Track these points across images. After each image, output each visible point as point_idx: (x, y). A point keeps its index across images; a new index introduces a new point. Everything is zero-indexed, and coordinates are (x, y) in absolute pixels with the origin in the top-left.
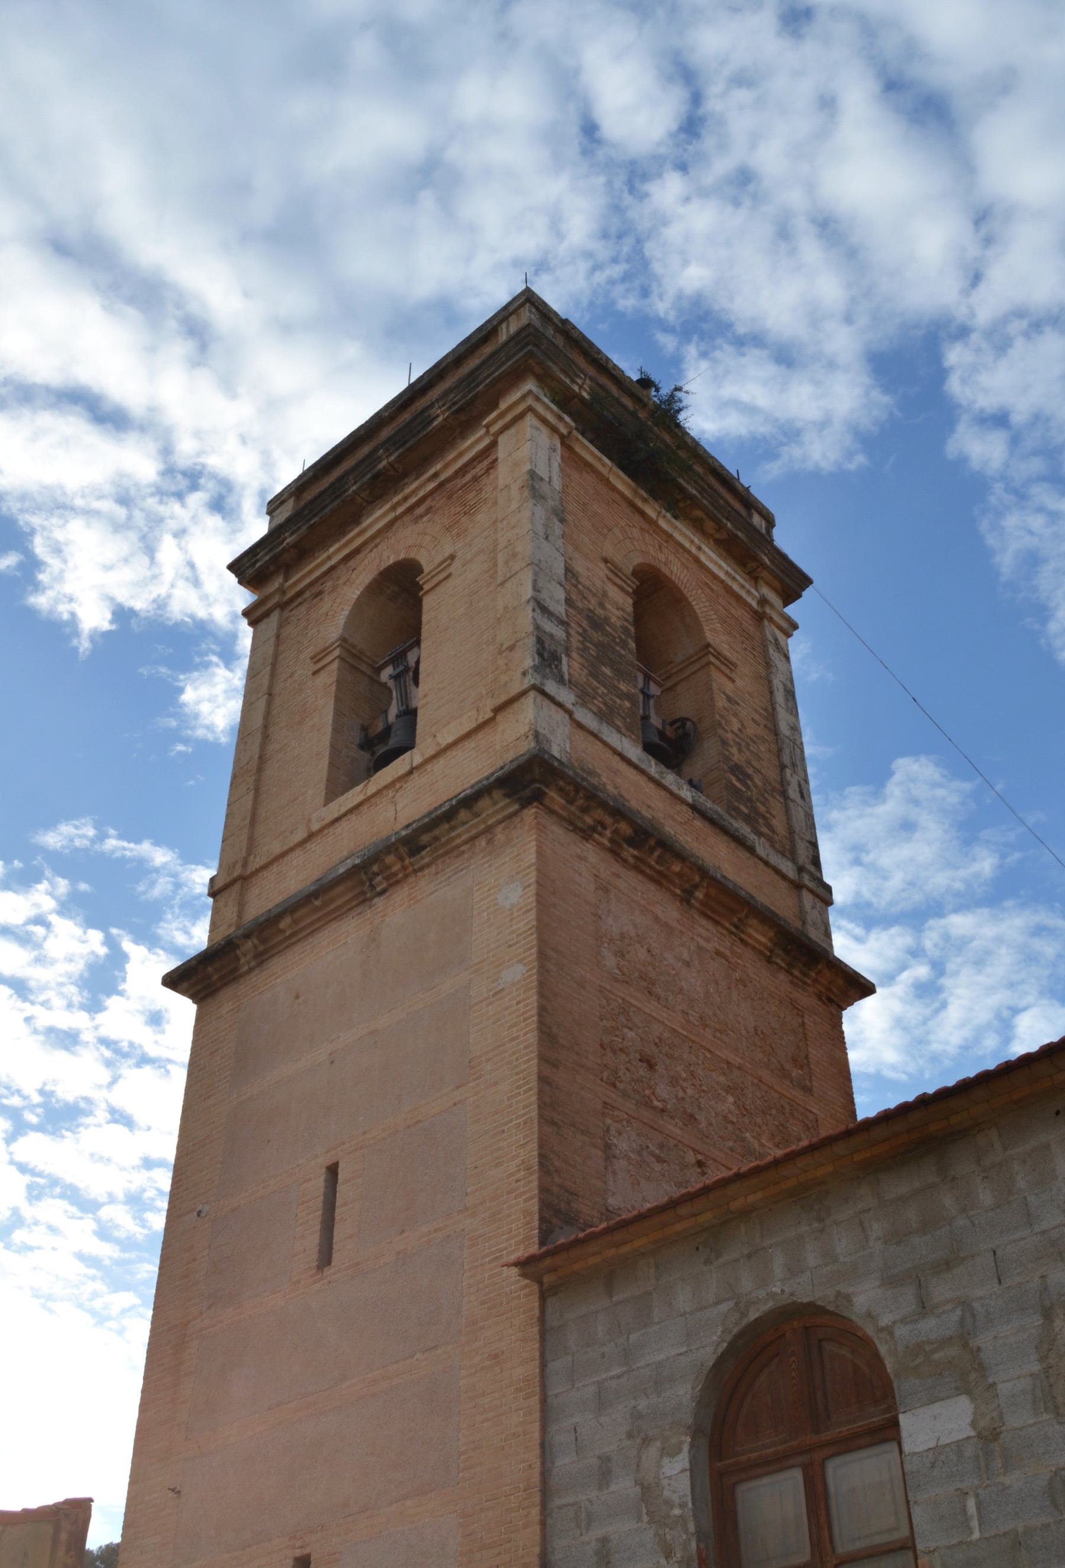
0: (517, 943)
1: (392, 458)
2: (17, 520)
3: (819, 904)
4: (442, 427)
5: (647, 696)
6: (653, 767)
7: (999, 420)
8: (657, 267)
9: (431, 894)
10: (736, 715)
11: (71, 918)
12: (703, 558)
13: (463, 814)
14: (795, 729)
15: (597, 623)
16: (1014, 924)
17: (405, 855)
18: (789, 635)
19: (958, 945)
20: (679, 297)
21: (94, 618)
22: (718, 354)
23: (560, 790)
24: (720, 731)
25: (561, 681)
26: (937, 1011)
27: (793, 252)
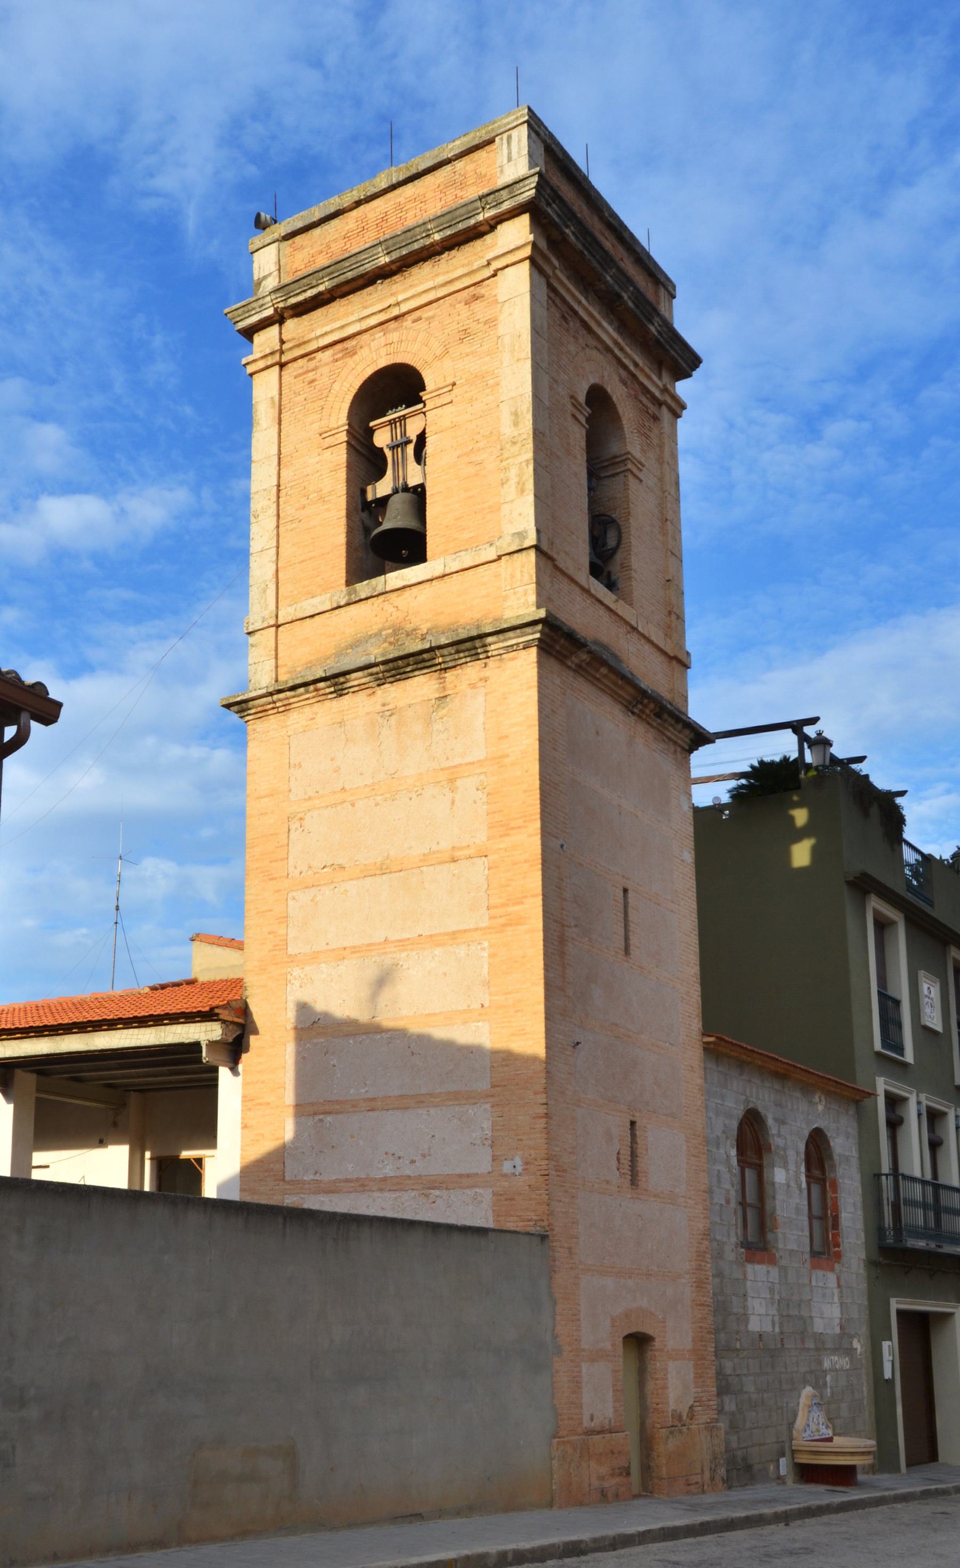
13: (680, 726)
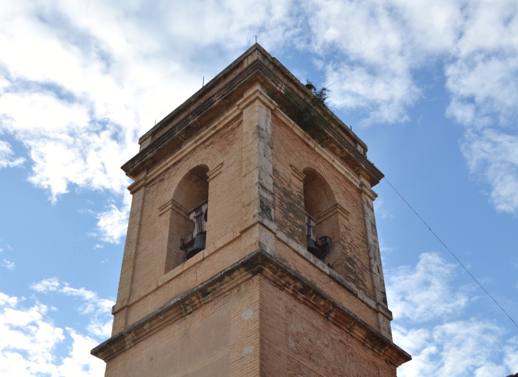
0: (251, 336)
1: (195, 119)
2: (23, 143)
3: (386, 320)
4: (218, 106)
5: (309, 227)
6: (312, 258)
7: (471, 100)
8: (314, 30)
9: (212, 314)
10: (349, 235)
11: (48, 322)
12: (335, 165)
13: (227, 279)
14: (376, 241)
15: (287, 194)
16: (475, 328)
17: (201, 297)
18: (373, 200)
19: (448, 337)
20: (324, 43)
21: (59, 188)
22: (341, 70)
23: (270, 268)
24: (342, 242)
25: (271, 219)
26: (440, 367)
27: (377, 23)
